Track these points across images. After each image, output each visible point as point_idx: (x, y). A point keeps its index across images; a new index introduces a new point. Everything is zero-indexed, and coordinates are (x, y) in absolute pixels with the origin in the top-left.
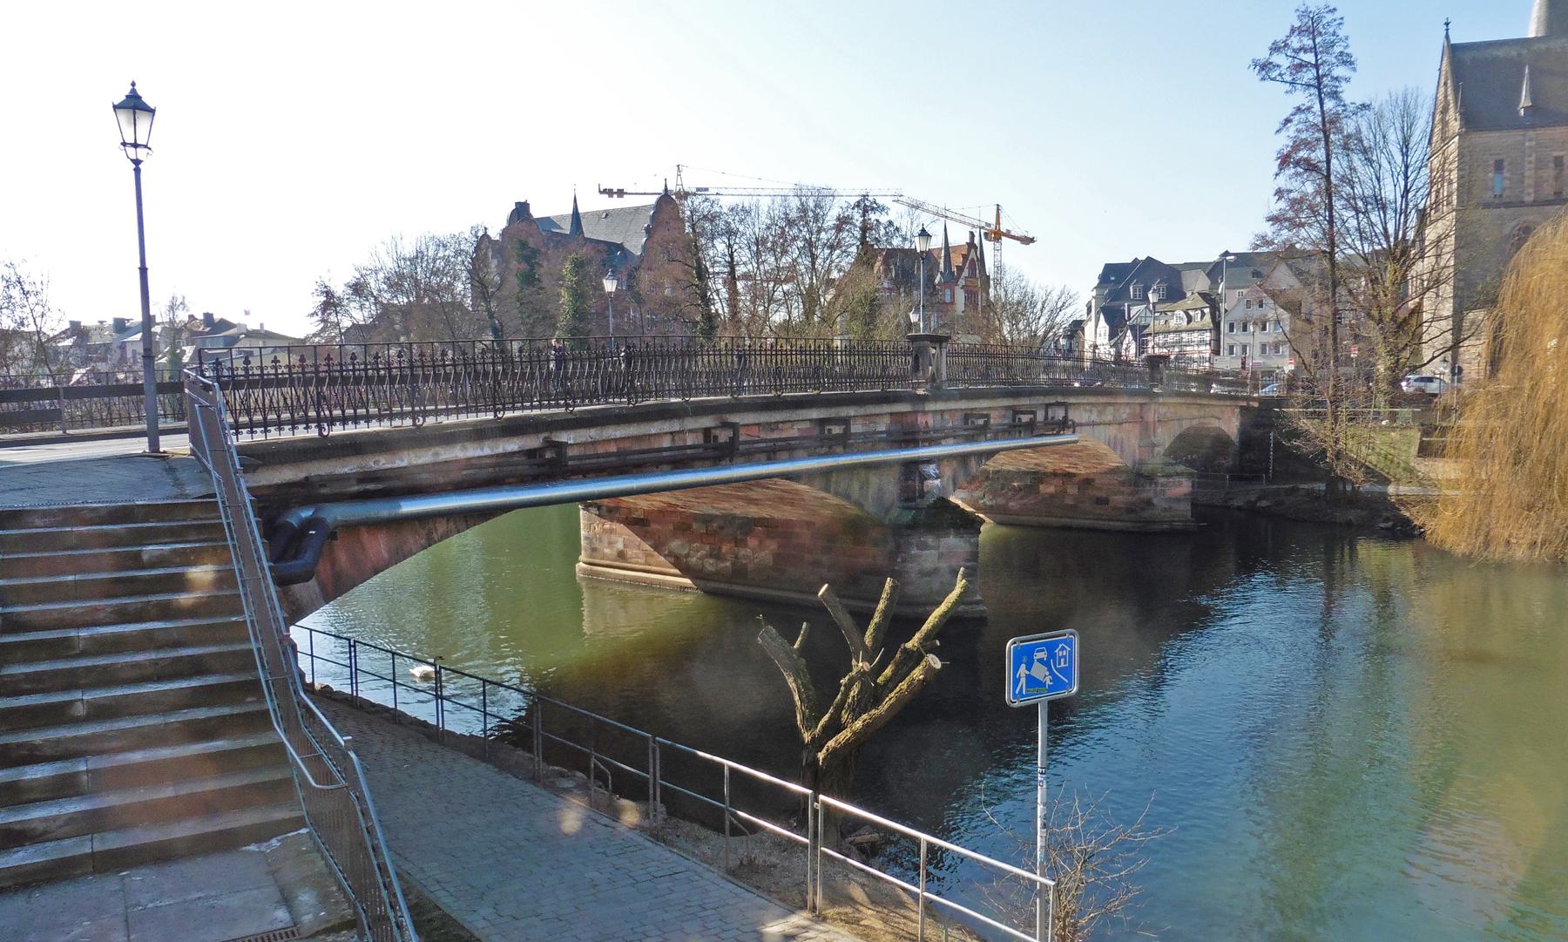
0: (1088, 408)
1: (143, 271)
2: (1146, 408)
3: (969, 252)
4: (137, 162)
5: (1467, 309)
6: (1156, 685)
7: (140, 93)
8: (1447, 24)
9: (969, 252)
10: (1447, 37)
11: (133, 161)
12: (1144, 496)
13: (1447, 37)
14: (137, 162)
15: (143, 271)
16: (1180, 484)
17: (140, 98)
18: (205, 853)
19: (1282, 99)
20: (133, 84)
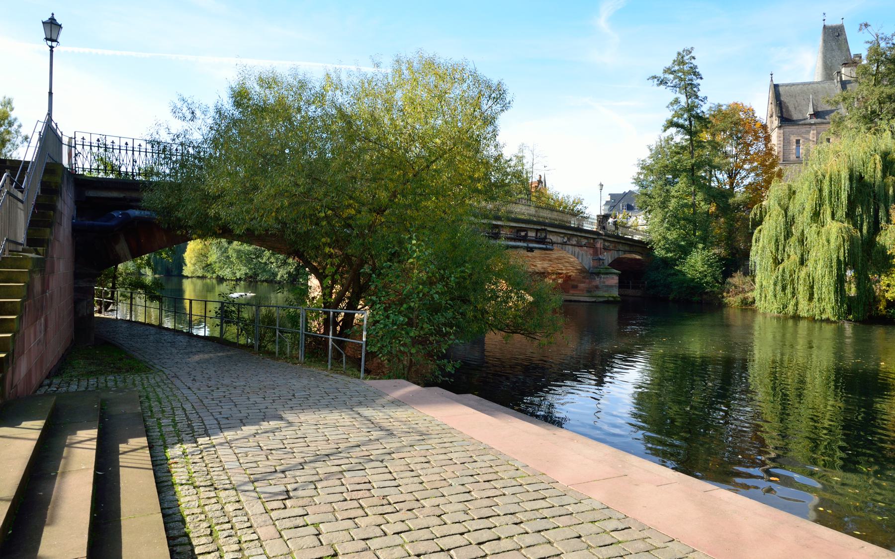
0: (562, 235)
1: (51, 94)
2: (596, 241)
3: (539, 184)
4: (52, 47)
5: (683, 148)
6: (600, 383)
7: (55, 18)
8: (772, 75)
9: (539, 184)
10: (772, 80)
11: (50, 46)
12: (594, 284)
13: (772, 80)
14: (52, 47)
15: (51, 94)
16: (613, 278)
17: (55, 20)
18: (171, 540)
19: (668, 94)
20: (53, 14)
